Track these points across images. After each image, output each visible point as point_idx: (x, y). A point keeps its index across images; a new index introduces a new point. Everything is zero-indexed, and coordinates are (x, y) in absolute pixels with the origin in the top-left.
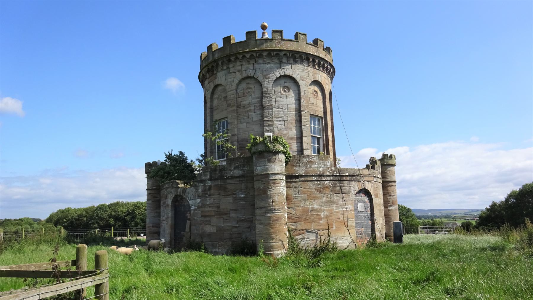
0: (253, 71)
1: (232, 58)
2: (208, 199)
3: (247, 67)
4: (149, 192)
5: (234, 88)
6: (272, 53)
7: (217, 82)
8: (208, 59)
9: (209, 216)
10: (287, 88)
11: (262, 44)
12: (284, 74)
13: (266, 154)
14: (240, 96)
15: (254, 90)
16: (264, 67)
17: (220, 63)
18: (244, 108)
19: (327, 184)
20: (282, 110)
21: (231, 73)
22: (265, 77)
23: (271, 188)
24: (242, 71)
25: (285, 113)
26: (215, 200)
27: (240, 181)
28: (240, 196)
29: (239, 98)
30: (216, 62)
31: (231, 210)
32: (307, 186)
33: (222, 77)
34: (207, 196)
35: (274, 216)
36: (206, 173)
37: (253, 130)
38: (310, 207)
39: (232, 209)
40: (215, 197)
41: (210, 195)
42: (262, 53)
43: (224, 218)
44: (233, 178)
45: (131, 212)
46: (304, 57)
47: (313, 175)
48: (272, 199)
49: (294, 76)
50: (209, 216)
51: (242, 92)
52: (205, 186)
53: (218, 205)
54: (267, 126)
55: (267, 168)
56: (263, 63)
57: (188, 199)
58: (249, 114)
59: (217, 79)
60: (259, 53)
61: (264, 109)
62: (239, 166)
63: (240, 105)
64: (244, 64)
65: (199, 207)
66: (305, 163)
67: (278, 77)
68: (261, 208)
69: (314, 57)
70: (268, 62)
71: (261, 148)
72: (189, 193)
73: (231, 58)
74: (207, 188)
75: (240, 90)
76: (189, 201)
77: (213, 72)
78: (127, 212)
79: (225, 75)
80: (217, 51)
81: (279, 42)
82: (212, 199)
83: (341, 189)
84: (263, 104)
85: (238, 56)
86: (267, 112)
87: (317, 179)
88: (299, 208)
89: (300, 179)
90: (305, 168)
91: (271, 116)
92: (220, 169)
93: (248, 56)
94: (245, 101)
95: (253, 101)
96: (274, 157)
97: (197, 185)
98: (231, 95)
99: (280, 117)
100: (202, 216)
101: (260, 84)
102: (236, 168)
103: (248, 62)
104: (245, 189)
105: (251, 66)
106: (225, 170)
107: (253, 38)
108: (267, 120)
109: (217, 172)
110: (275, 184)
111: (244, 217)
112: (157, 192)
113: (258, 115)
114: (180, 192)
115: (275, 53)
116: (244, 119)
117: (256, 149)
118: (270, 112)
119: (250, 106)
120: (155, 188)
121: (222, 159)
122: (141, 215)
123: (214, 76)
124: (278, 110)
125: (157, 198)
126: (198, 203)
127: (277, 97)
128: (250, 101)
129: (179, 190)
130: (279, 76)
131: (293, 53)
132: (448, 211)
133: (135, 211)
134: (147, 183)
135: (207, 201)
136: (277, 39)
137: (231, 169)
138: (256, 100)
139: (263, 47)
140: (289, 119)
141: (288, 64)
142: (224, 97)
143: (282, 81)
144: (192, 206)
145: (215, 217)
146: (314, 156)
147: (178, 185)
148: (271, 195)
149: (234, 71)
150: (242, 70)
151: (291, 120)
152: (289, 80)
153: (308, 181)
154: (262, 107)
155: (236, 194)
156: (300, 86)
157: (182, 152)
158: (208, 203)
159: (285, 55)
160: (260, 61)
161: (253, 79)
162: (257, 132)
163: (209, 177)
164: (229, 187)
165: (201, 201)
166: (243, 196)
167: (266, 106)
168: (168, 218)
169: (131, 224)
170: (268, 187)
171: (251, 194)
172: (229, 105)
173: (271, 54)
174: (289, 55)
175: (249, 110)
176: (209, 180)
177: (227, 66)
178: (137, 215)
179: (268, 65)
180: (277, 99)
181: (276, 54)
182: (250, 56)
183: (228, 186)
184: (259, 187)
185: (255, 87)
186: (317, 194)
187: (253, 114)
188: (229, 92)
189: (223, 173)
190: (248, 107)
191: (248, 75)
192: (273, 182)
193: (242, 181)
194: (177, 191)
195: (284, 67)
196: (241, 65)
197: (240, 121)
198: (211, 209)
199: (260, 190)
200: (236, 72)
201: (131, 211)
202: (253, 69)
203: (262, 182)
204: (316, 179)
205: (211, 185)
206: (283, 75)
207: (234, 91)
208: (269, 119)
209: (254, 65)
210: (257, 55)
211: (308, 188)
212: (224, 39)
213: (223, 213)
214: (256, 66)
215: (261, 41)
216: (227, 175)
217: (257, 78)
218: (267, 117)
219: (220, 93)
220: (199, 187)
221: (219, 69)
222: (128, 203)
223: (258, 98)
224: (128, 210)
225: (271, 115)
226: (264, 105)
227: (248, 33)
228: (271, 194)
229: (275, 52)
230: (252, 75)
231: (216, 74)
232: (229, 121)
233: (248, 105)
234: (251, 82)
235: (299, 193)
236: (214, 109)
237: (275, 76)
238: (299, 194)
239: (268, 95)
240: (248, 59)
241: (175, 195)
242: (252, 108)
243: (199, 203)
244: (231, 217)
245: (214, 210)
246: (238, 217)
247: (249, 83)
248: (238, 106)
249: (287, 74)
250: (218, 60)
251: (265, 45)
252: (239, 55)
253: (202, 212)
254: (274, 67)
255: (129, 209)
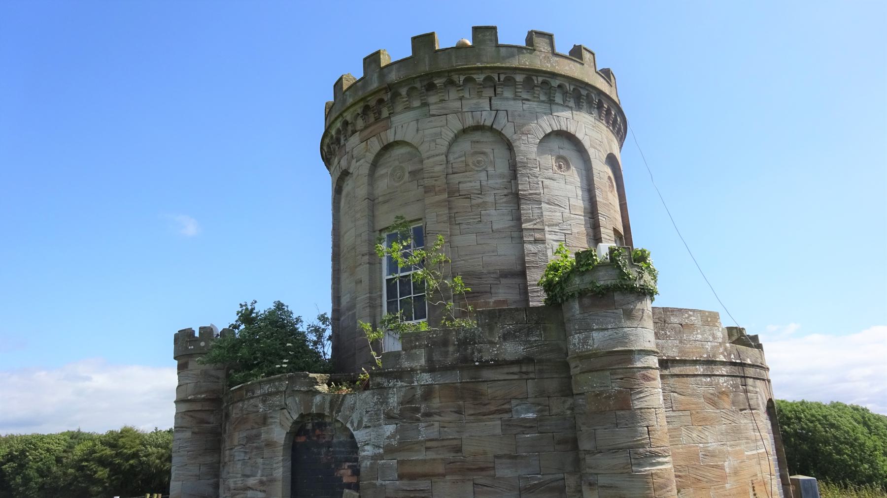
0: (491, 115)
1: (438, 82)
2: (423, 424)
3: (475, 104)
4: (184, 407)
5: (444, 149)
6: (534, 78)
7: (390, 136)
8: (364, 86)
9: (425, 476)
10: (563, 162)
11: (512, 56)
12: (559, 129)
13: (617, 297)
14: (455, 170)
15: (492, 158)
16: (516, 106)
17: (404, 91)
18: (469, 198)
19: (723, 383)
20: (557, 207)
21: (434, 115)
22: (519, 129)
23: (641, 392)
24: (462, 112)
25: (565, 215)
26: (446, 429)
27: (521, 372)
28: (523, 416)
29: (453, 173)
30: (390, 90)
31: (497, 457)
32: (688, 388)
33: (406, 125)
34: (419, 415)
35: (656, 474)
36: (414, 351)
37: (493, 252)
38: (701, 445)
39: (500, 453)
40: (447, 419)
41: (428, 415)
42: (512, 76)
43: (476, 482)
44: (499, 364)
45: (17, 456)
46: (594, 98)
47: (696, 361)
48: (645, 424)
49: (580, 136)
50: (425, 476)
51: (462, 162)
52: (413, 388)
53: (455, 442)
54: (530, 242)
55: (625, 336)
56: (514, 99)
57: (349, 426)
58: (482, 212)
59: (393, 130)
60: (505, 73)
61: (523, 201)
62: (515, 332)
63: (459, 191)
64: (467, 95)
65: (390, 450)
66: (677, 330)
67: (547, 133)
68: (615, 450)
69: (612, 104)
70: (525, 97)
71: (604, 279)
72: (353, 409)
73: (435, 82)
74: (419, 392)
75: (456, 156)
76: (354, 433)
77: (380, 113)
78: (8, 455)
79: (417, 120)
80: (394, 67)
81: (548, 57)
82: (437, 424)
83: (748, 399)
84: (519, 190)
85: (455, 77)
86: (527, 209)
87: (704, 370)
88: (678, 449)
89: (671, 369)
90: (678, 342)
91: (538, 220)
92: (459, 340)
93: (480, 78)
94: (470, 182)
95: (490, 182)
96: (639, 306)
97: (385, 385)
98: (435, 166)
99: (556, 225)
100: (401, 477)
101: (509, 146)
102: (505, 337)
103: (478, 92)
104: (536, 397)
105: (485, 104)
106: (475, 343)
107: (491, 40)
108: (531, 227)
109: (451, 349)
110: (650, 381)
111: (539, 476)
112: (207, 408)
113: (503, 215)
114: (321, 406)
115: (540, 79)
116: (468, 224)
117: (592, 282)
118: (536, 211)
119: (484, 195)
120: (203, 396)
121: (415, 319)
122: (38, 462)
123: (380, 124)
124: (551, 208)
125: (209, 423)
126: (388, 438)
127: (546, 178)
128: (484, 183)
129: (318, 399)
130: (549, 130)
131: (577, 86)
132: (452, 441)
133: (28, 454)
134: (177, 384)
135: (420, 431)
136: (543, 51)
137: (493, 339)
138: (496, 182)
139: (514, 63)
140: (575, 230)
141: (566, 109)
142: (409, 173)
143: (555, 144)
144: (366, 448)
145: (448, 478)
146: (691, 313)
147: (313, 386)
148: (643, 411)
149: (439, 111)
150: (464, 110)
151: (578, 233)
152: (566, 144)
153: (687, 376)
154: (516, 198)
155: (511, 411)
156: (592, 160)
157: (283, 305)
158: (420, 438)
159: (560, 86)
160: (508, 93)
161: (488, 134)
162: (505, 255)
163: (423, 362)
164: (489, 391)
165: (397, 431)
166: (530, 415)
167: (526, 195)
168: (272, 481)
169: (14, 479)
170: (632, 389)
171: (555, 411)
172: (428, 190)
173: (533, 80)
174: (568, 89)
175: (481, 204)
176: (423, 371)
177: (422, 100)
178: (30, 460)
179: (524, 104)
180: (547, 182)
181: (544, 82)
182: (485, 79)
183: (484, 387)
184: (606, 389)
185: (495, 151)
186: (710, 410)
187: (493, 212)
188: (428, 158)
189: (469, 351)
190: (479, 196)
191: (478, 122)
192: (644, 375)
193: (526, 373)
194: (308, 405)
195: (557, 111)
196: (461, 99)
197: (457, 227)
198: (431, 455)
199: (609, 397)
200: (446, 115)
201: (16, 453)
202: (491, 110)
203: (611, 374)
204: (702, 370)
205: (432, 384)
206: (558, 131)
207: (444, 157)
208: (535, 227)
209: (492, 101)
210: (502, 79)
211: (691, 395)
212: (414, 39)
213: (474, 467)
214: (496, 103)
215: (510, 49)
216: (482, 357)
217: (500, 130)
218: (531, 221)
219: (397, 163)
220: (391, 391)
221: (399, 107)
222: (12, 437)
223: (501, 176)
224: (11, 450)
225: (540, 218)
226: (522, 192)
227: (476, 30)
228: (641, 409)
229: (540, 76)
230: (488, 123)
231: (389, 118)
232: (430, 227)
233: (480, 192)
234: (485, 140)
235: (674, 409)
236: (376, 201)
237: (541, 130)
238: (673, 411)
239: (528, 171)
240: (478, 87)
241: (302, 416)
242: (490, 199)
243: (393, 436)
244: (498, 478)
245: (442, 459)
246: (520, 478)
247: (477, 142)
248: (453, 192)
249: (565, 129)
250: (400, 84)
251: (519, 59)
252: (457, 76)
253: (401, 463)
254: (538, 110)
255: (13, 448)
